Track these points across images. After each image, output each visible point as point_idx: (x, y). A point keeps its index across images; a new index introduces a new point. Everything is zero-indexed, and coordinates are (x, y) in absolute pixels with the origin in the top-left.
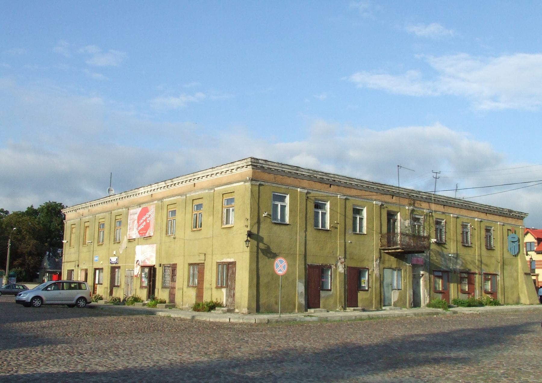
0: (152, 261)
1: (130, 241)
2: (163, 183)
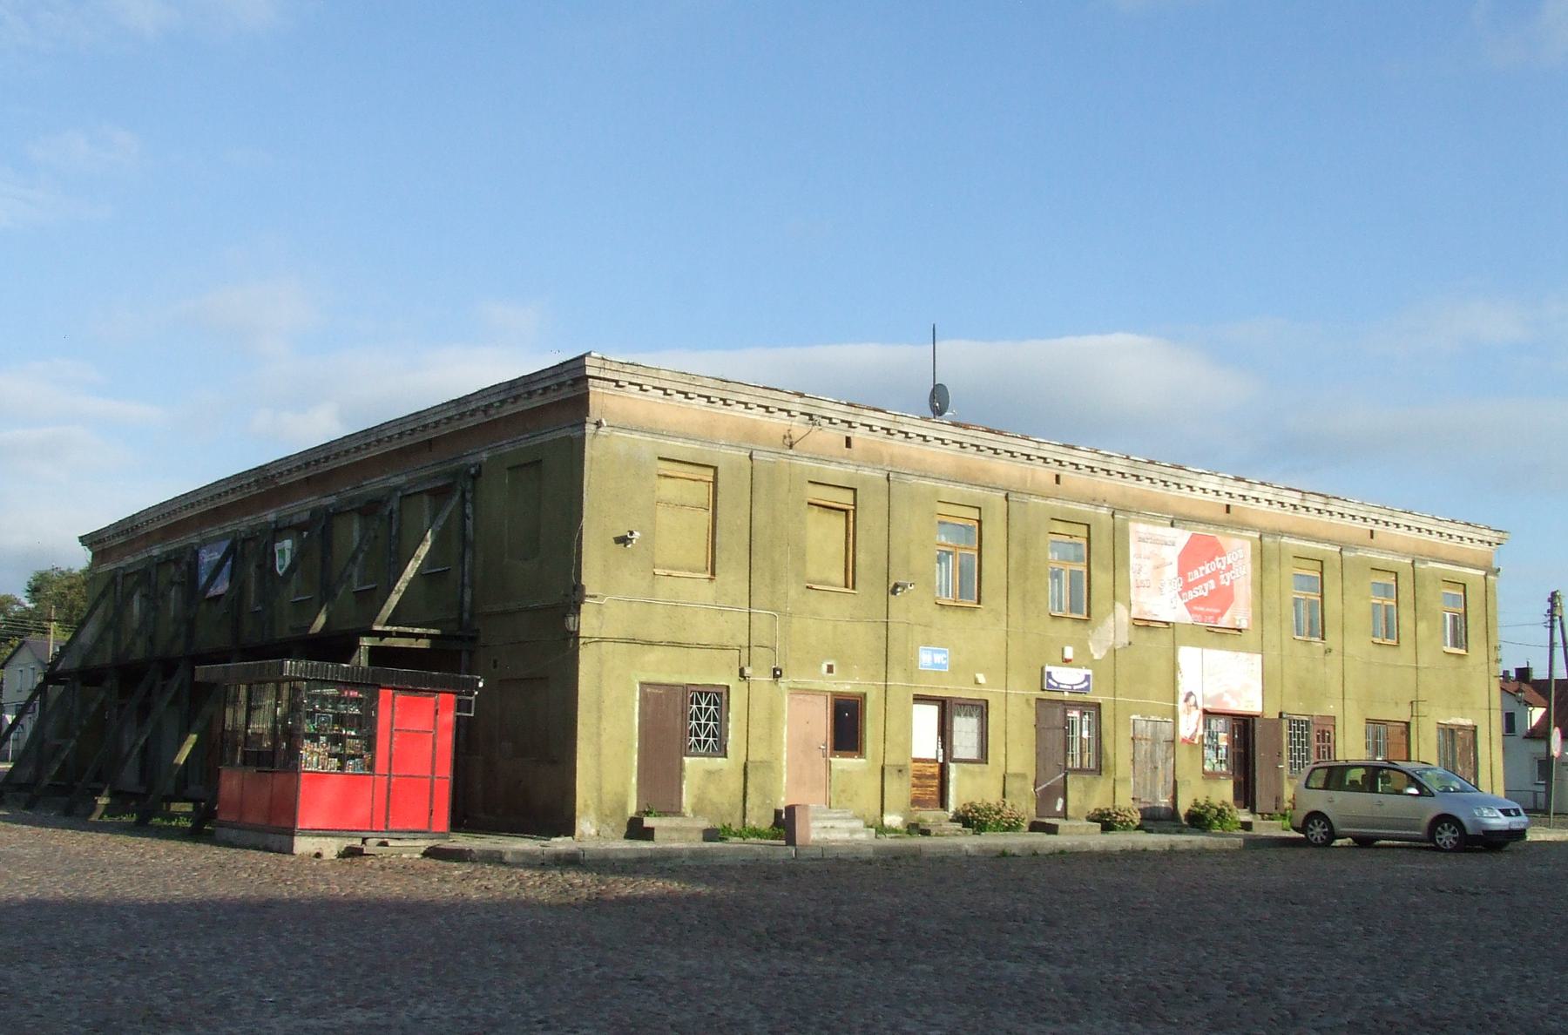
0: (1250, 703)
1: (1144, 625)
2: (1299, 495)
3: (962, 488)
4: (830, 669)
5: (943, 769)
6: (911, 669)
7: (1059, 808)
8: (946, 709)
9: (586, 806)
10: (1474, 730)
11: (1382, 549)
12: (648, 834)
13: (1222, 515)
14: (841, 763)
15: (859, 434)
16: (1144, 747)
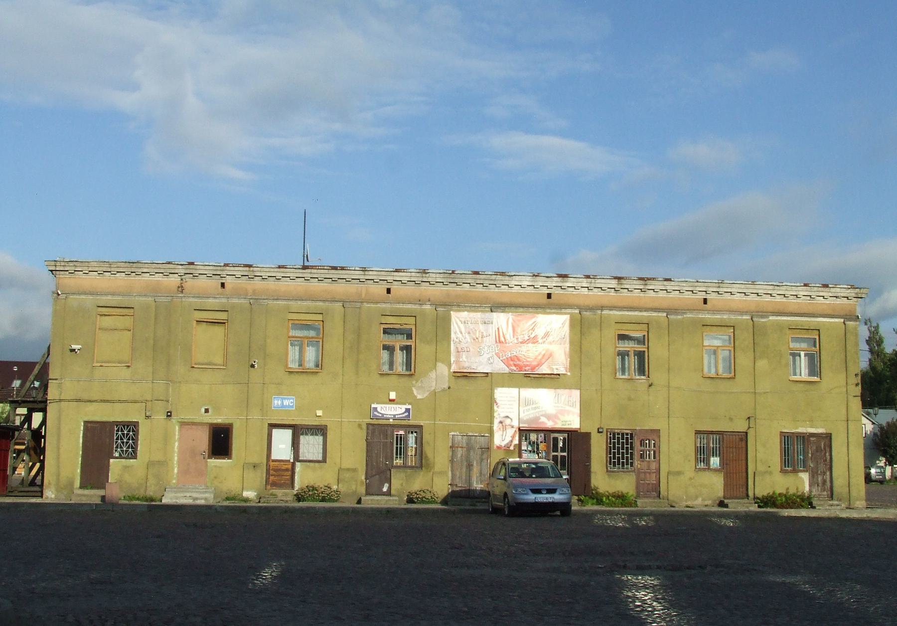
3: (309, 303)
4: (207, 411)
5: (293, 465)
6: (264, 407)
7: (385, 489)
8: (298, 431)
9: (50, 484)
10: (828, 437)
11: (715, 311)
12: (726, 506)
13: (545, 300)
14: (216, 462)
15: (229, 281)
16: (460, 452)
